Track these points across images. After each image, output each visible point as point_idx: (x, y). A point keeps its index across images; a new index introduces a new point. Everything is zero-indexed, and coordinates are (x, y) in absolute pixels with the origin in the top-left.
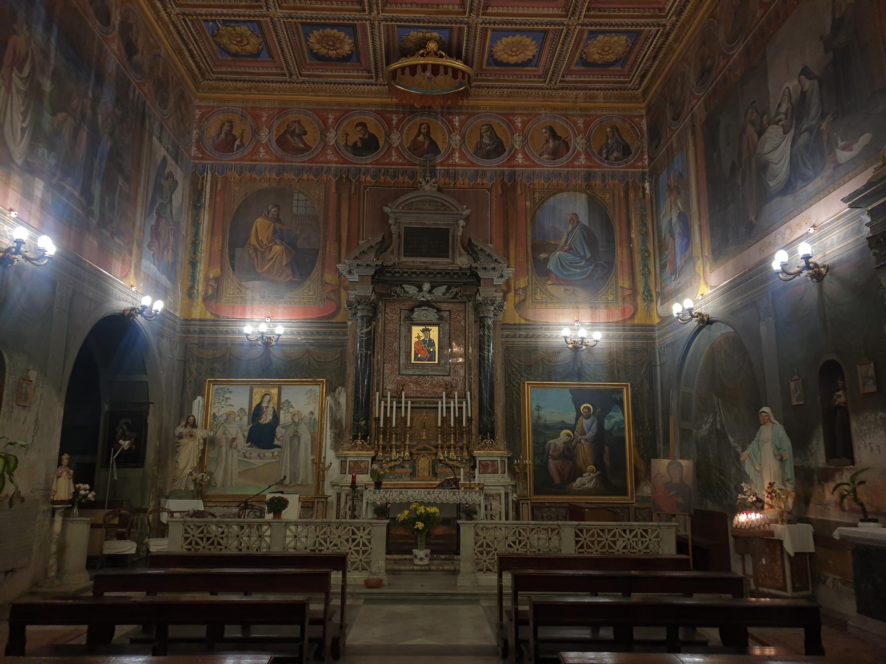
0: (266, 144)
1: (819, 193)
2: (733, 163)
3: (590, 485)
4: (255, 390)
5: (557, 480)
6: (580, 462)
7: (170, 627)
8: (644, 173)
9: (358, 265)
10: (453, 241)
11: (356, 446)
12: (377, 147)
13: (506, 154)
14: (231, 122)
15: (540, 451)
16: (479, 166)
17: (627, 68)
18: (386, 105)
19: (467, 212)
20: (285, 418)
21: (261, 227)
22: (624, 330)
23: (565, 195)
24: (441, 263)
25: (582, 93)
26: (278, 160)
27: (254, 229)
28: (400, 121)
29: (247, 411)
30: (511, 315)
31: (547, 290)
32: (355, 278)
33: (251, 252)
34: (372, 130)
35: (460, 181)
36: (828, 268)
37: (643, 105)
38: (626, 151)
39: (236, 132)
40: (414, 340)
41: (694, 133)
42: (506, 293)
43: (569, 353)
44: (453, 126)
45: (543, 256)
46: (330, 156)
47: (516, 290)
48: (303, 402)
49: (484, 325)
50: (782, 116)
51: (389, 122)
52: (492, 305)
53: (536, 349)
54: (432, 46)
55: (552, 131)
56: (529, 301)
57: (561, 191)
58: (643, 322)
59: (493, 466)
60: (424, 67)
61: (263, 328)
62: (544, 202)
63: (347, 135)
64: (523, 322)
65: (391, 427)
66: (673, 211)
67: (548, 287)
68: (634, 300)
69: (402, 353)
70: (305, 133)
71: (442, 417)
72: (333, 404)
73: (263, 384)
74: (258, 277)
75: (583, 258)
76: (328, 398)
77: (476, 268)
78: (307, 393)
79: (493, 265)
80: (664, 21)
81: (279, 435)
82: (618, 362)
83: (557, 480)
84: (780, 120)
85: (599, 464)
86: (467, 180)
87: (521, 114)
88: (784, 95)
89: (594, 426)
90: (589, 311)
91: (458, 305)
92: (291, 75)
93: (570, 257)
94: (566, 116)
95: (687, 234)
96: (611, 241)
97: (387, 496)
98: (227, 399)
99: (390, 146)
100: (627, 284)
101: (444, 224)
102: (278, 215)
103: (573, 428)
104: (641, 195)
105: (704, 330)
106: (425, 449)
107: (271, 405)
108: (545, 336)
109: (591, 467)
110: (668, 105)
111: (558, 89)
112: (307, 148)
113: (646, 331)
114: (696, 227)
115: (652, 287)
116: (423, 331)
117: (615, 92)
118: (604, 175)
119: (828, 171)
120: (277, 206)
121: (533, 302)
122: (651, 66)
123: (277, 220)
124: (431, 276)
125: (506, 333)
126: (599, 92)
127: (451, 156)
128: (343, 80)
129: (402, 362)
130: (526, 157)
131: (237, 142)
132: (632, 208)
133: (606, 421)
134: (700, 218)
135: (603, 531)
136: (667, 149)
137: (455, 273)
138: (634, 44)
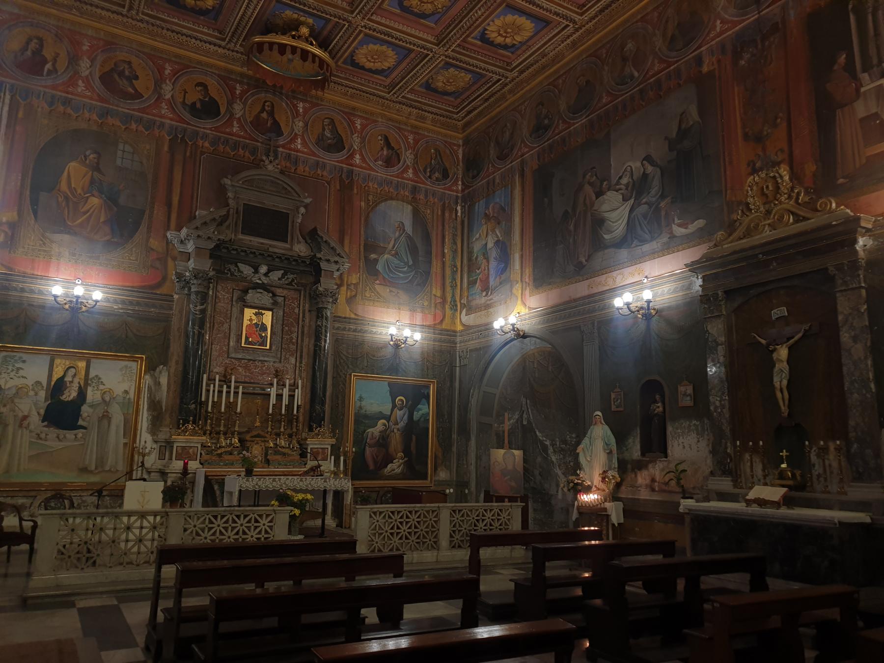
0: (239, 118)
1: (654, 253)
2: (566, 212)
3: (398, 471)
4: (58, 361)
5: (372, 467)
6: (392, 449)
7: (703, 578)
8: (457, 196)
9: (199, 236)
10: (293, 226)
11: (185, 431)
12: (218, 113)
13: (345, 151)
14: (41, 40)
15: (360, 440)
16: (319, 157)
17: (459, 100)
18: (231, 72)
19: (308, 201)
20: (92, 395)
21: (75, 173)
22: (434, 333)
23: (394, 203)
24: (278, 247)
25: (415, 111)
26: (101, 100)
27: (65, 173)
28: (244, 92)
29: (45, 384)
30: (343, 309)
31: (375, 289)
32: (190, 247)
33: (60, 199)
34: (213, 93)
35: (301, 168)
36: (657, 311)
37: (461, 136)
38: (445, 175)
39: (48, 53)
40: (246, 322)
41: (522, 175)
42: (339, 286)
43: (390, 350)
44: (297, 111)
45: (373, 256)
46: (165, 110)
47: (348, 285)
48: (116, 379)
49: (322, 316)
50: (622, 186)
51: (232, 90)
52: (332, 297)
53: (362, 343)
54: (304, 31)
55: (386, 139)
56: (359, 297)
57: (392, 199)
58: (449, 328)
59: (323, 453)
60: (294, 49)
61: (393, 330)
62: (376, 205)
63: (186, 92)
64: (353, 316)
65: (207, 411)
66: (490, 237)
67: (376, 286)
68: (444, 308)
69: (232, 335)
70: (137, 78)
71: (213, 402)
72: (152, 384)
73: (68, 356)
74: (69, 230)
75: (406, 264)
76: (147, 377)
77: (320, 259)
78: (121, 370)
79: (337, 259)
80: (508, 74)
81: (85, 415)
82: (428, 361)
83: (372, 467)
84: (620, 189)
85: (407, 451)
86: (307, 169)
87: (360, 117)
88: (625, 170)
89: (406, 417)
90: (408, 313)
91: (293, 292)
92: (131, 8)
93: (396, 261)
94: (399, 129)
95: (505, 258)
96: (429, 253)
97: (260, 483)
98: (18, 369)
99: (232, 115)
100: (439, 294)
101: (284, 208)
102: (98, 163)
103: (388, 418)
104: (454, 216)
105: (515, 342)
106: (258, 436)
107: (76, 380)
108: (371, 332)
109: (400, 454)
110: (492, 145)
111: (396, 102)
112: (138, 95)
113: (450, 335)
114: (517, 256)
115: (458, 299)
116: (256, 314)
117: (442, 118)
118: (426, 191)
119: (665, 239)
120: (96, 152)
121: (362, 299)
122: (480, 106)
123: (96, 168)
124: (270, 259)
125: (337, 325)
126: (429, 115)
127: (293, 140)
128: (190, 32)
129: (232, 344)
130: (363, 159)
131: (48, 66)
132: (447, 226)
133: (415, 413)
134: (522, 249)
135: (393, 513)
136: (488, 183)
137: (295, 260)
138: (474, 83)
